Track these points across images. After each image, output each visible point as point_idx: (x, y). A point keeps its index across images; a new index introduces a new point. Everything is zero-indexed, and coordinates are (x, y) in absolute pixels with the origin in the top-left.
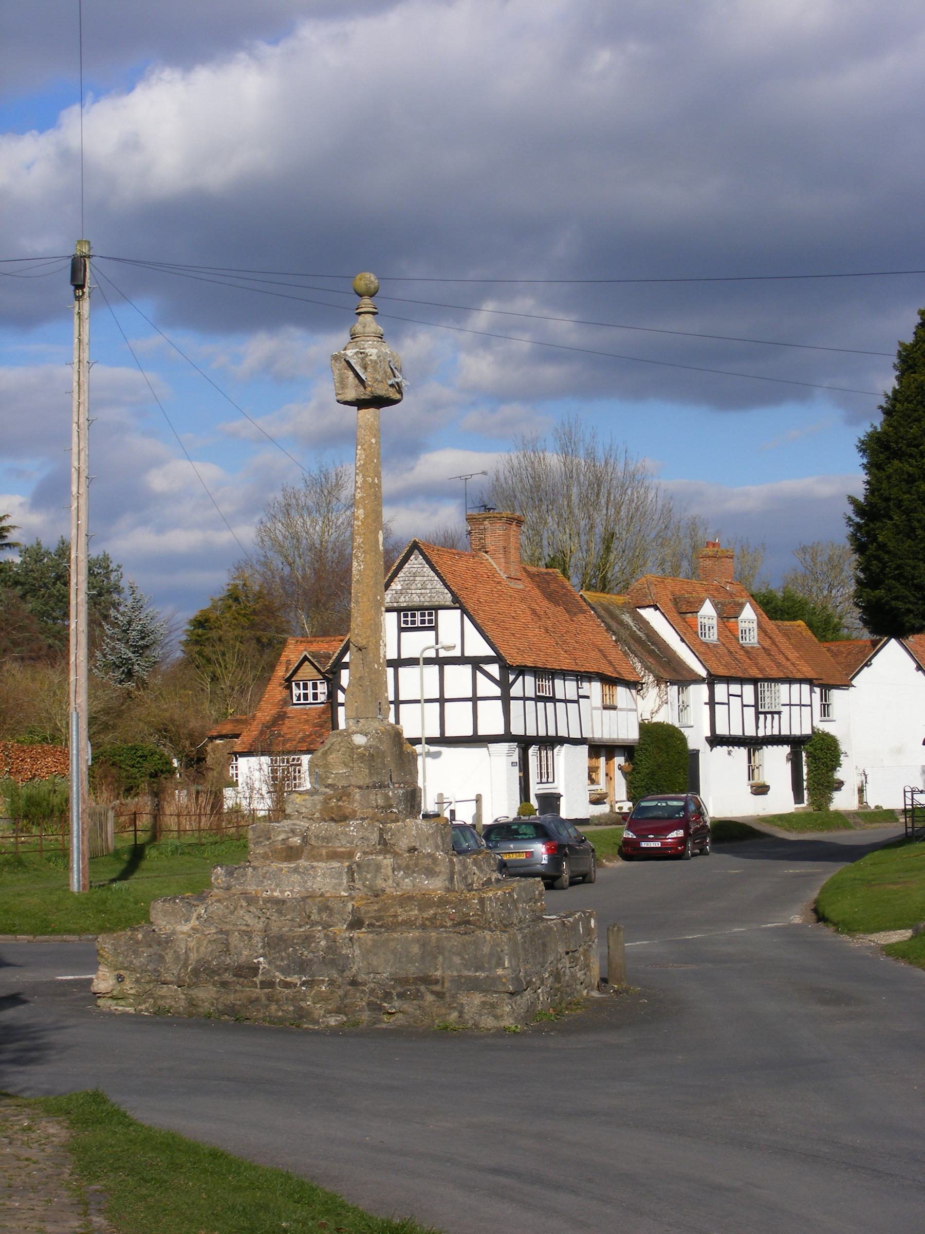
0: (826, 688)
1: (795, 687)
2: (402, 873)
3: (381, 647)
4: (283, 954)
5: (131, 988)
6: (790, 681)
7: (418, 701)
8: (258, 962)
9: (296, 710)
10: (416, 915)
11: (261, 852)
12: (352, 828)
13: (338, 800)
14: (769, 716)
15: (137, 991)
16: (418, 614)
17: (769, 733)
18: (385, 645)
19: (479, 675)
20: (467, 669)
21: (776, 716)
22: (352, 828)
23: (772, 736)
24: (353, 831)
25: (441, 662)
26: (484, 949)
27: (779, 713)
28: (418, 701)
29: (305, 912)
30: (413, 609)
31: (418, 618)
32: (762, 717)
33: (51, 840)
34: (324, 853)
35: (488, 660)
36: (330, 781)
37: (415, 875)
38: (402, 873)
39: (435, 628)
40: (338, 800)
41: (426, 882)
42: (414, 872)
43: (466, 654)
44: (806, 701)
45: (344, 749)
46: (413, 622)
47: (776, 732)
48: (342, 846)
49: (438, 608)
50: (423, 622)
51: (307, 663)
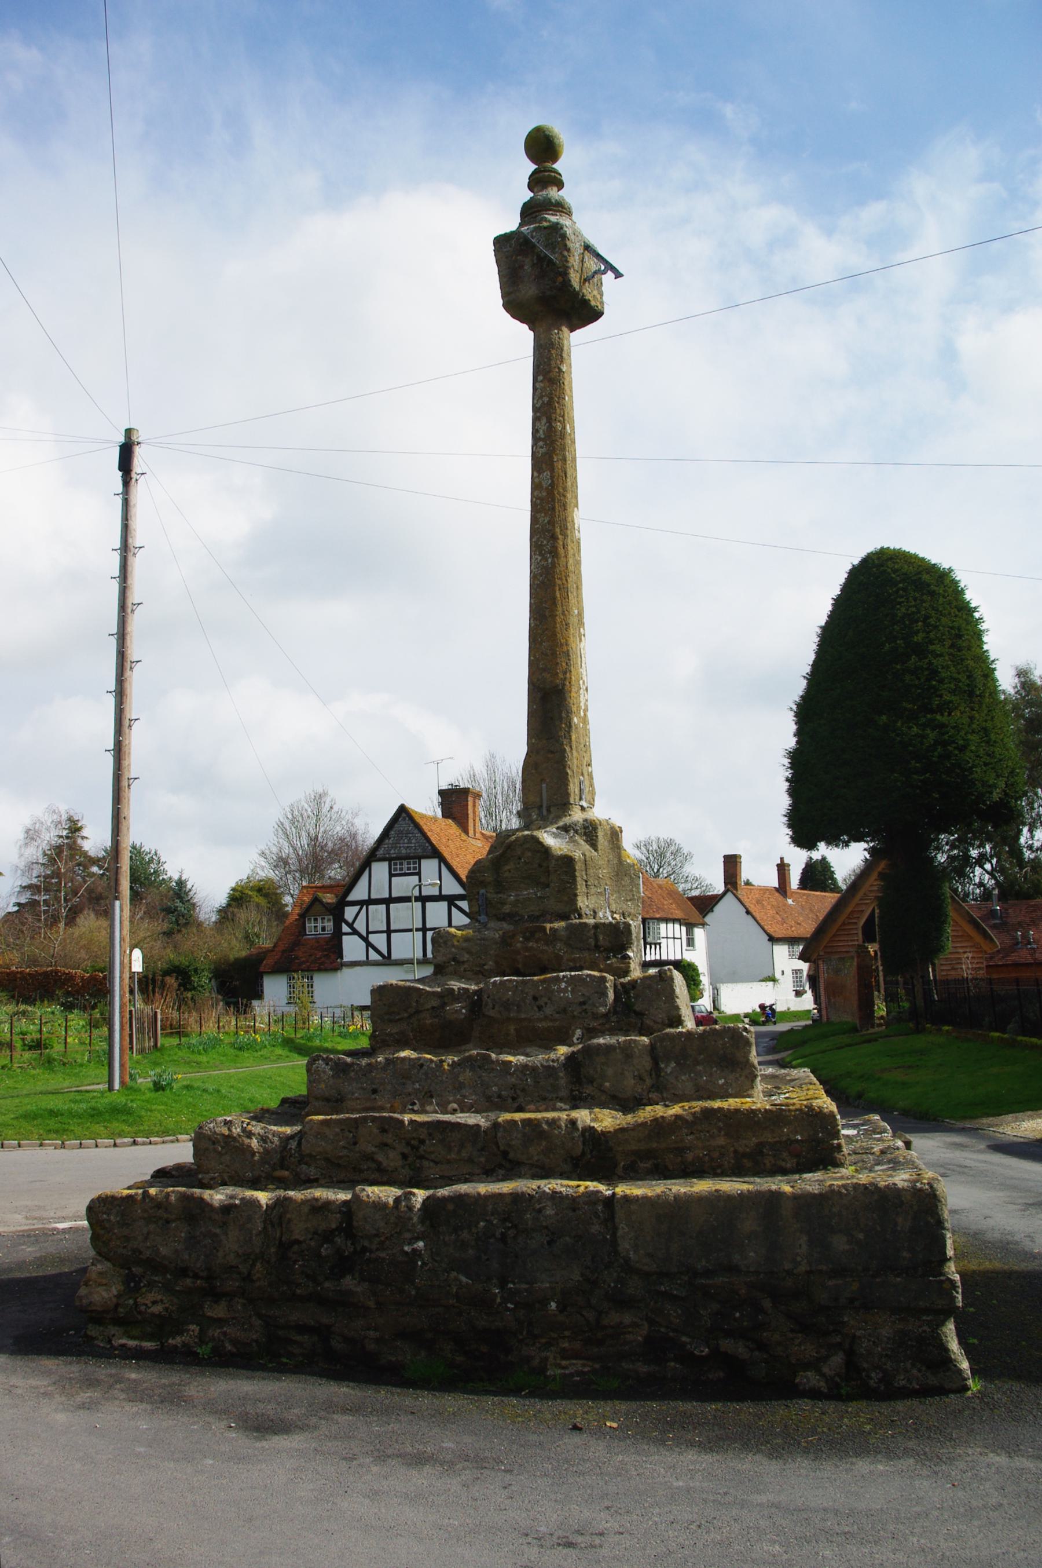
0: (690, 926)
1: (670, 925)
2: (673, 1065)
3: (582, 691)
4: (465, 1235)
5: (154, 1303)
6: (667, 920)
7: (410, 930)
8: (414, 1250)
9: (309, 939)
10: (722, 1147)
11: (394, 1031)
12: (563, 985)
13: (527, 939)
14: (653, 946)
15: (166, 1309)
16: (405, 862)
17: (653, 958)
18: (587, 689)
19: (454, 910)
20: (444, 905)
21: (658, 947)
22: (563, 985)
23: (656, 961)
24: (565, 990)
25: (423, 900)
26: (900, 1220)
27: (660, 944)
28: (410, 930)
29: (497, 1144)
30: (400, 858)
31: (405, 866)
32: (648, 947)
33: (749, 1224)
34: (512, 1031)
35: (461, 897)
36: (507, 909)
37: (700, 1068)
38: (673, 1065)
39: (419, 874)
40: (527, 939)
41: (722, 1081)
42: (697, 1063)
43: (443, 893)
44: (677, 935)
45: (529, 854)
46: (401, 869)
47: (658, 958)
48: (546, 1018)
49: (420, 858)
50: (409, 869)
51: (317, 903)
